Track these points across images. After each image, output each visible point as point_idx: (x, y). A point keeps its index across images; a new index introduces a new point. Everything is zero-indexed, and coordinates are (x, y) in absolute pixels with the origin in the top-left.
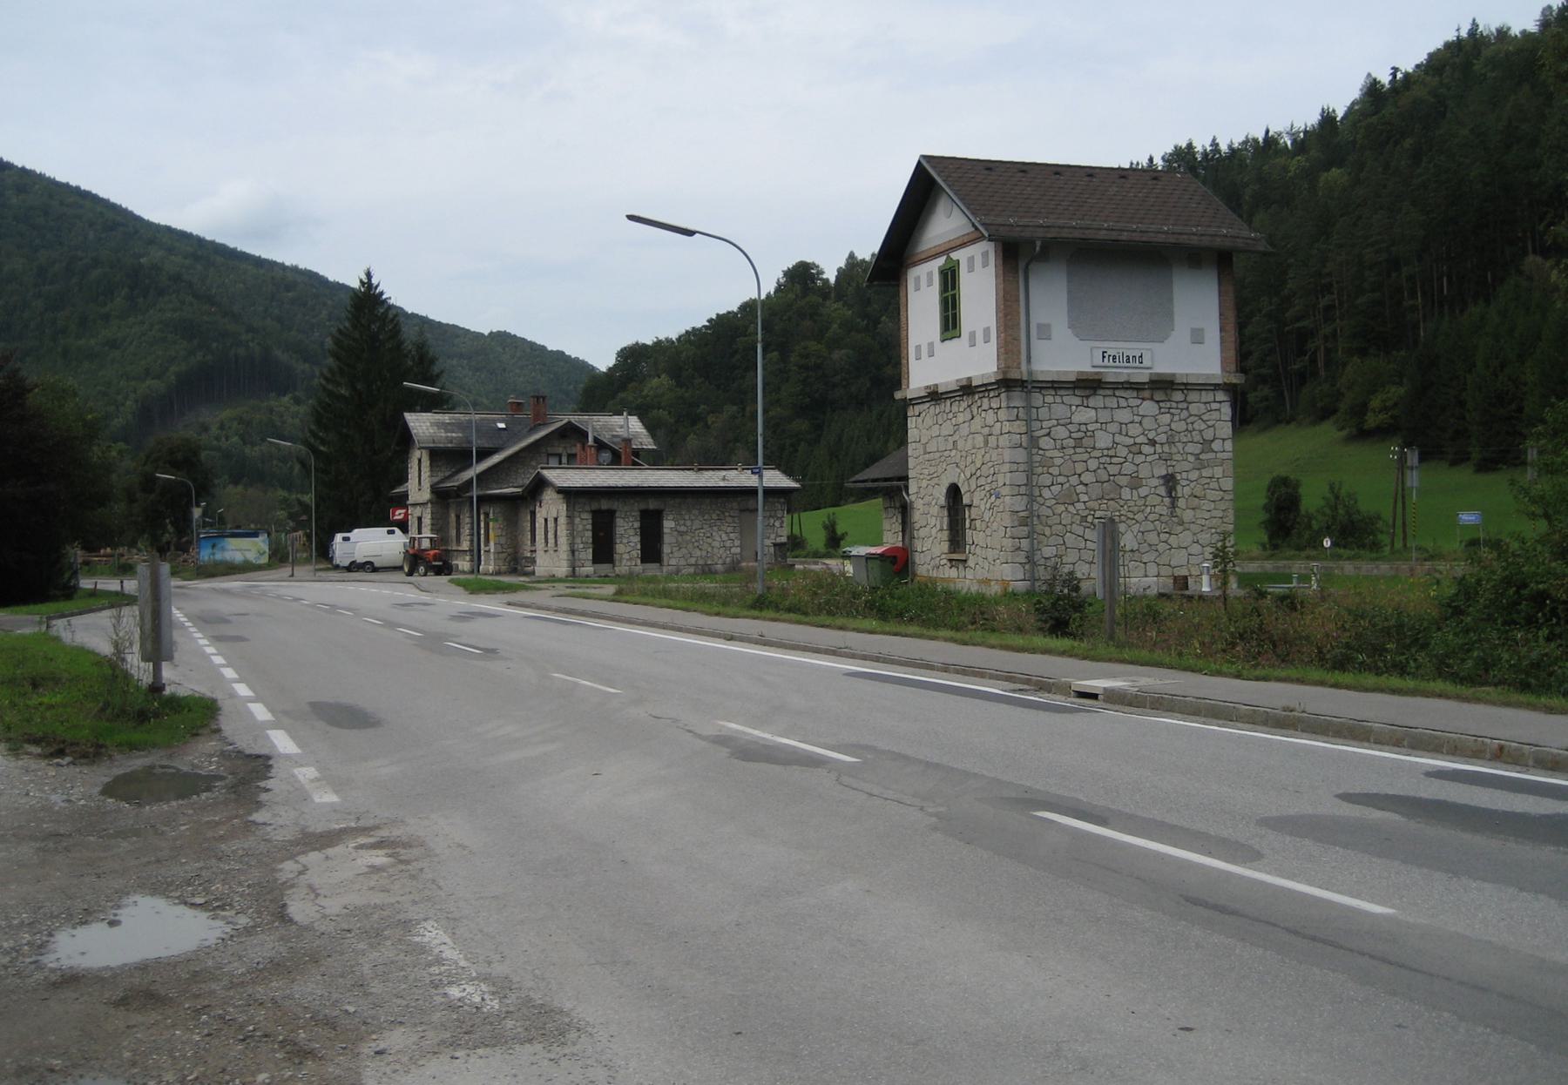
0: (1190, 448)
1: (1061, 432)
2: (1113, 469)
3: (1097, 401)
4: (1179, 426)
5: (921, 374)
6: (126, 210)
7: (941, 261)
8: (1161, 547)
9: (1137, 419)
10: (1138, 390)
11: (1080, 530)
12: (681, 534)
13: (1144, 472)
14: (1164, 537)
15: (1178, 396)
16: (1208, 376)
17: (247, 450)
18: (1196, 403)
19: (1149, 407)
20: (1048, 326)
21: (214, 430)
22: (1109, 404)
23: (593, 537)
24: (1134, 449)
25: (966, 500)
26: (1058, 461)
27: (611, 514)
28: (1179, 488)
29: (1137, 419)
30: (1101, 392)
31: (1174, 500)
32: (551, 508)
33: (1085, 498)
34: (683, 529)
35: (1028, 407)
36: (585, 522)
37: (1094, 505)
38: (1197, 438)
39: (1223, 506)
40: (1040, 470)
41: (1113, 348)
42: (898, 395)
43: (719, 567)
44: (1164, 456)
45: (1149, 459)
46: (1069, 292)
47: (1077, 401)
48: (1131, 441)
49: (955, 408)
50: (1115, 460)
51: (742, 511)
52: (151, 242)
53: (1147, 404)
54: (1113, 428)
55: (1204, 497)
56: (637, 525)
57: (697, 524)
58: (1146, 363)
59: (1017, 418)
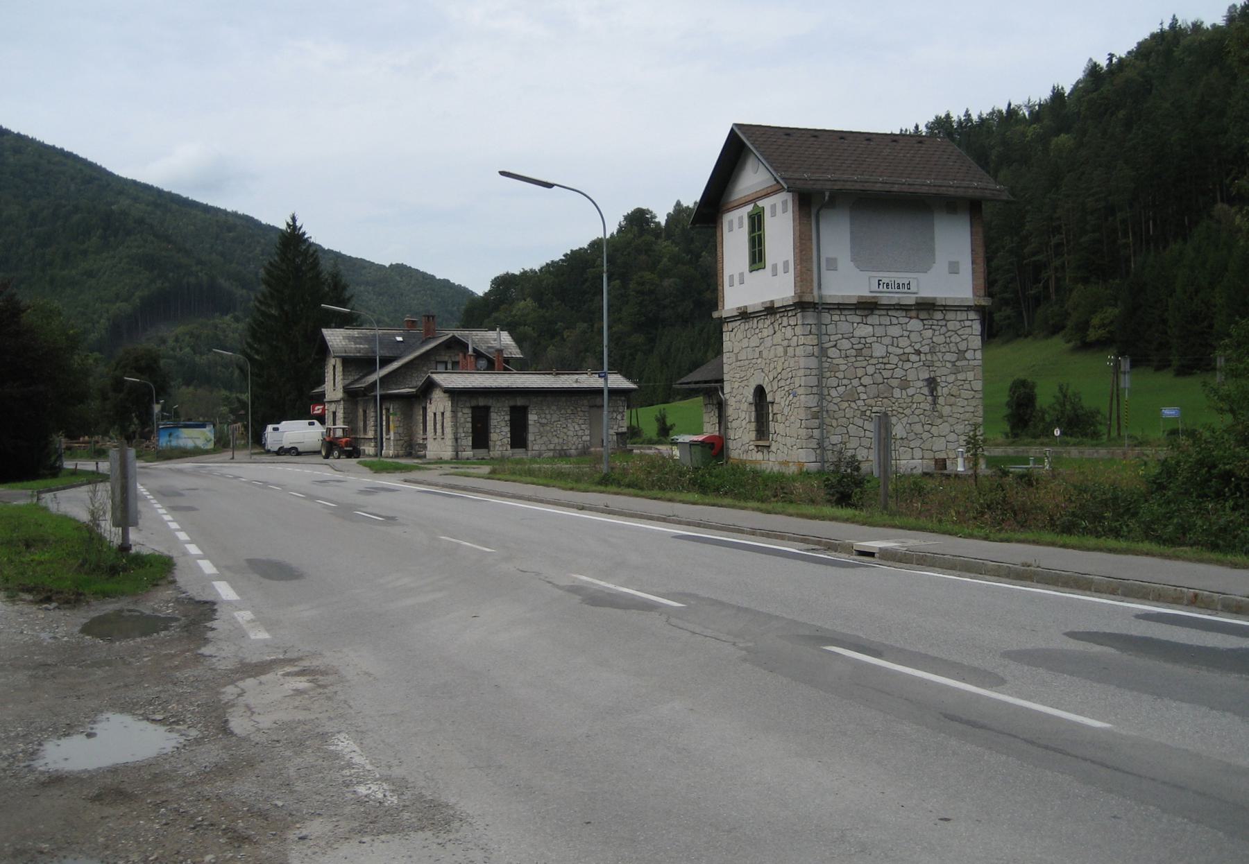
0: (948, 357)
1: (845, 344)
2: (887, 374)
3: (874, 319)
4: (939, 339)
5: (734, 298)
6: (100, 167)
7: (750, 208)
8: (925, 436)
9: (906, 333)
10: (906, 310)
11: (860, 422)
12: (543, 425)
13: (911, 376)
14: (927, 427)
15: (938, 315)
16: (962, 299)
17: (197, 358)
18: (953, 321)
19: (915, 324)
20: (835, 260)
21: (171, 342)
22: (883, 322)
23: (473, 427)
24: (903, 358)
25: (769, 398)
26: (843, 367)
27: (487, 409)
28: (939, 389)
29: (906, 333)
30: (877, 312)
31: (935, 398)
32: (439, 404)
33: (865, 397)
34: (544, 421)
35: (819, 324)
36: (466, 416)
37: (871, 402)
38: (954, 349)
39: (974, 403)
40: (828, 374)
41: (887, 277)
42: (715, 315)
43: (573, 452)
44: (927, 363)
45: (915, 365)
46: (852, 233)
47: (858, 319)
48: (901, 351)
49: (761, 325)
50: (888, 366)
51: (591, 407)
52: (120, 193)
53: (914, 322)
54: (887, 341)
55: (959, 396)
56: (507, 418)
57: (555, 417)
58: (913, 289)
59: (810, 333)
